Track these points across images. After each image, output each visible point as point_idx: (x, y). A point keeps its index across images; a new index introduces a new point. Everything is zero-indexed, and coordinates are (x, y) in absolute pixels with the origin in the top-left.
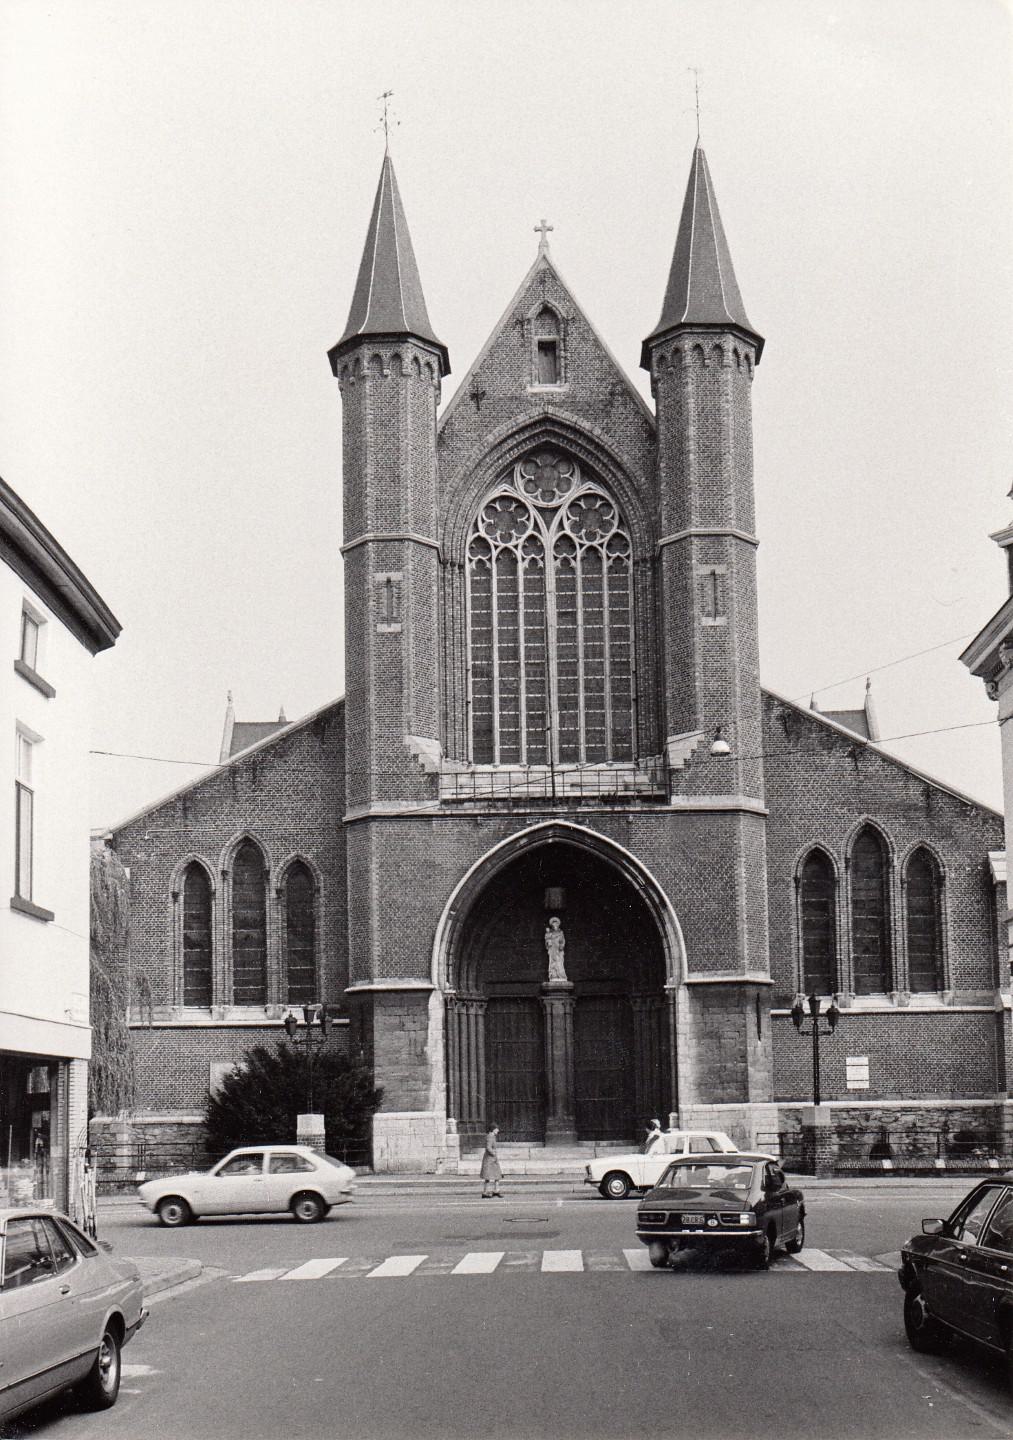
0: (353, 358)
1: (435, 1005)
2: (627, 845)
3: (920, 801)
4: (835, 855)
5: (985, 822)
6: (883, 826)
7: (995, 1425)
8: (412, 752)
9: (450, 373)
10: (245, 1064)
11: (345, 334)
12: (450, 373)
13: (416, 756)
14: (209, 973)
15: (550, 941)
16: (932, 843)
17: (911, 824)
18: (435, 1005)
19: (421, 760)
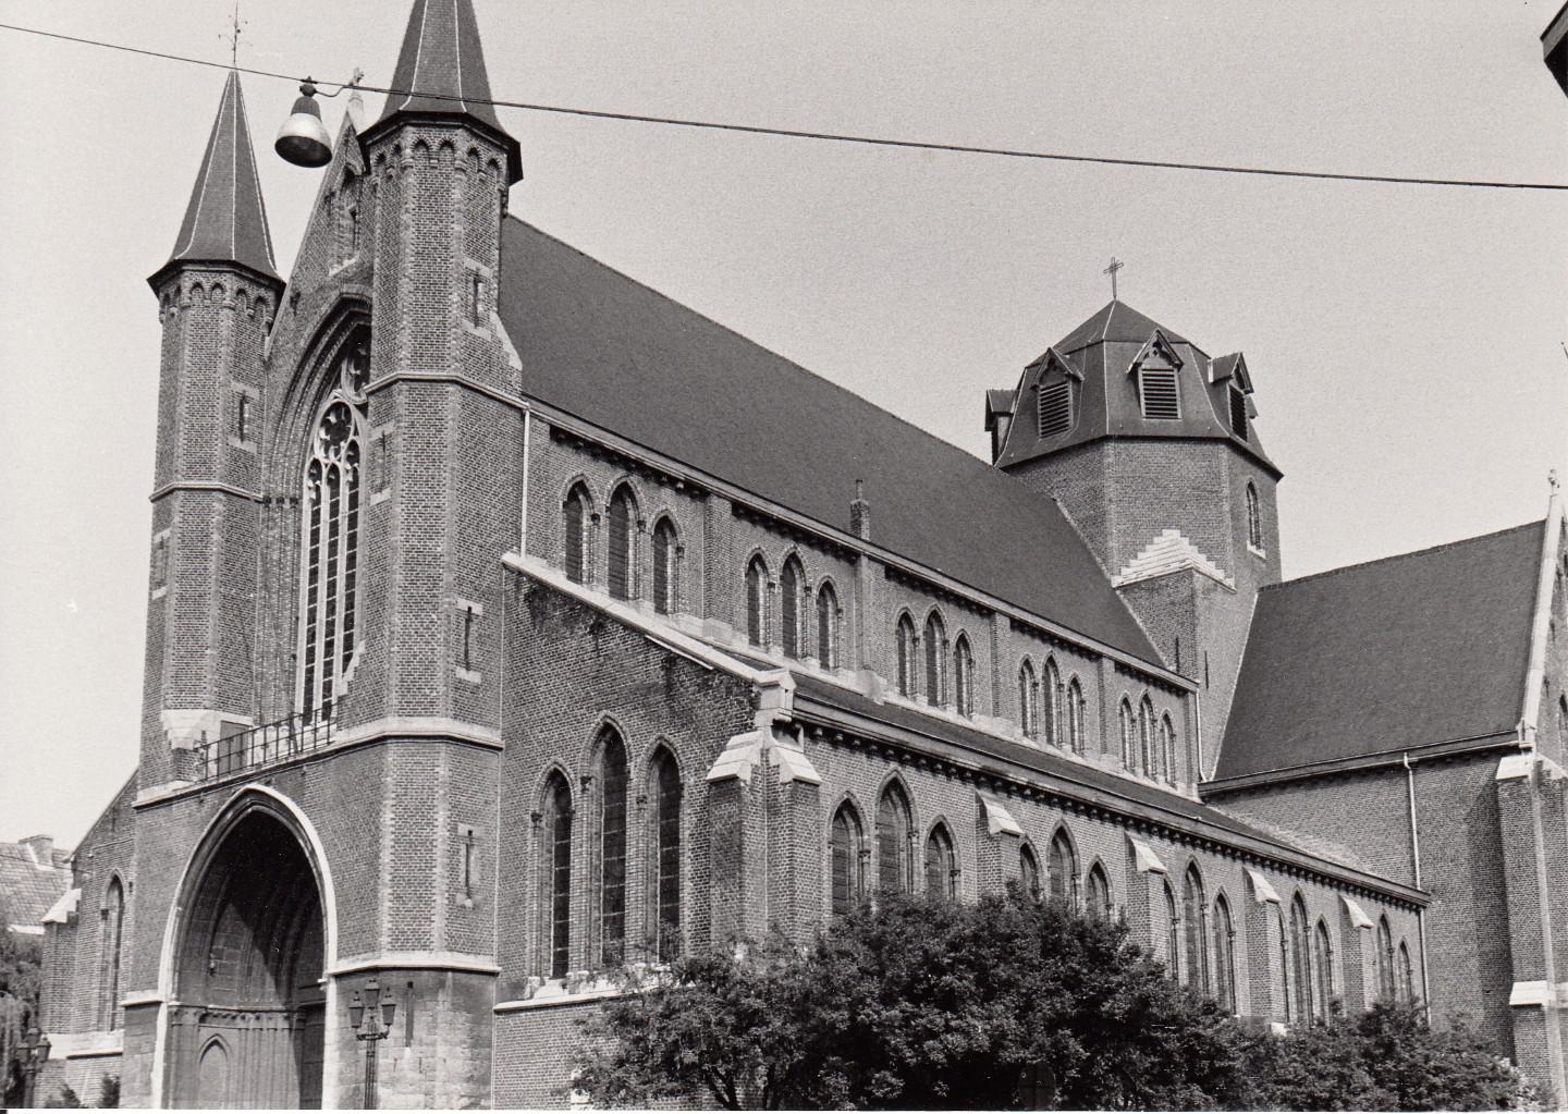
0: (392, 147)
1: (163, 1013)
2: (299, 803)
3: (657, 675)
4: (572, 776)
5: (729, 691)
6: (621, 723)
7: (1215, 809)
8: (165, 729)
9: (521, 177)
10: (815, 914)
11: (384, 112)
12: (521, 177)
13: (166, 733)
14: (677, 909)
15: (1342, 811)
16: (676, 740)
17: (652, 716)
18: (163, 1013)
19: (169, 736)
